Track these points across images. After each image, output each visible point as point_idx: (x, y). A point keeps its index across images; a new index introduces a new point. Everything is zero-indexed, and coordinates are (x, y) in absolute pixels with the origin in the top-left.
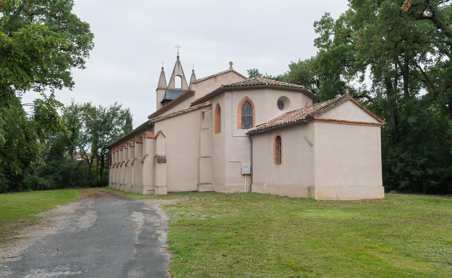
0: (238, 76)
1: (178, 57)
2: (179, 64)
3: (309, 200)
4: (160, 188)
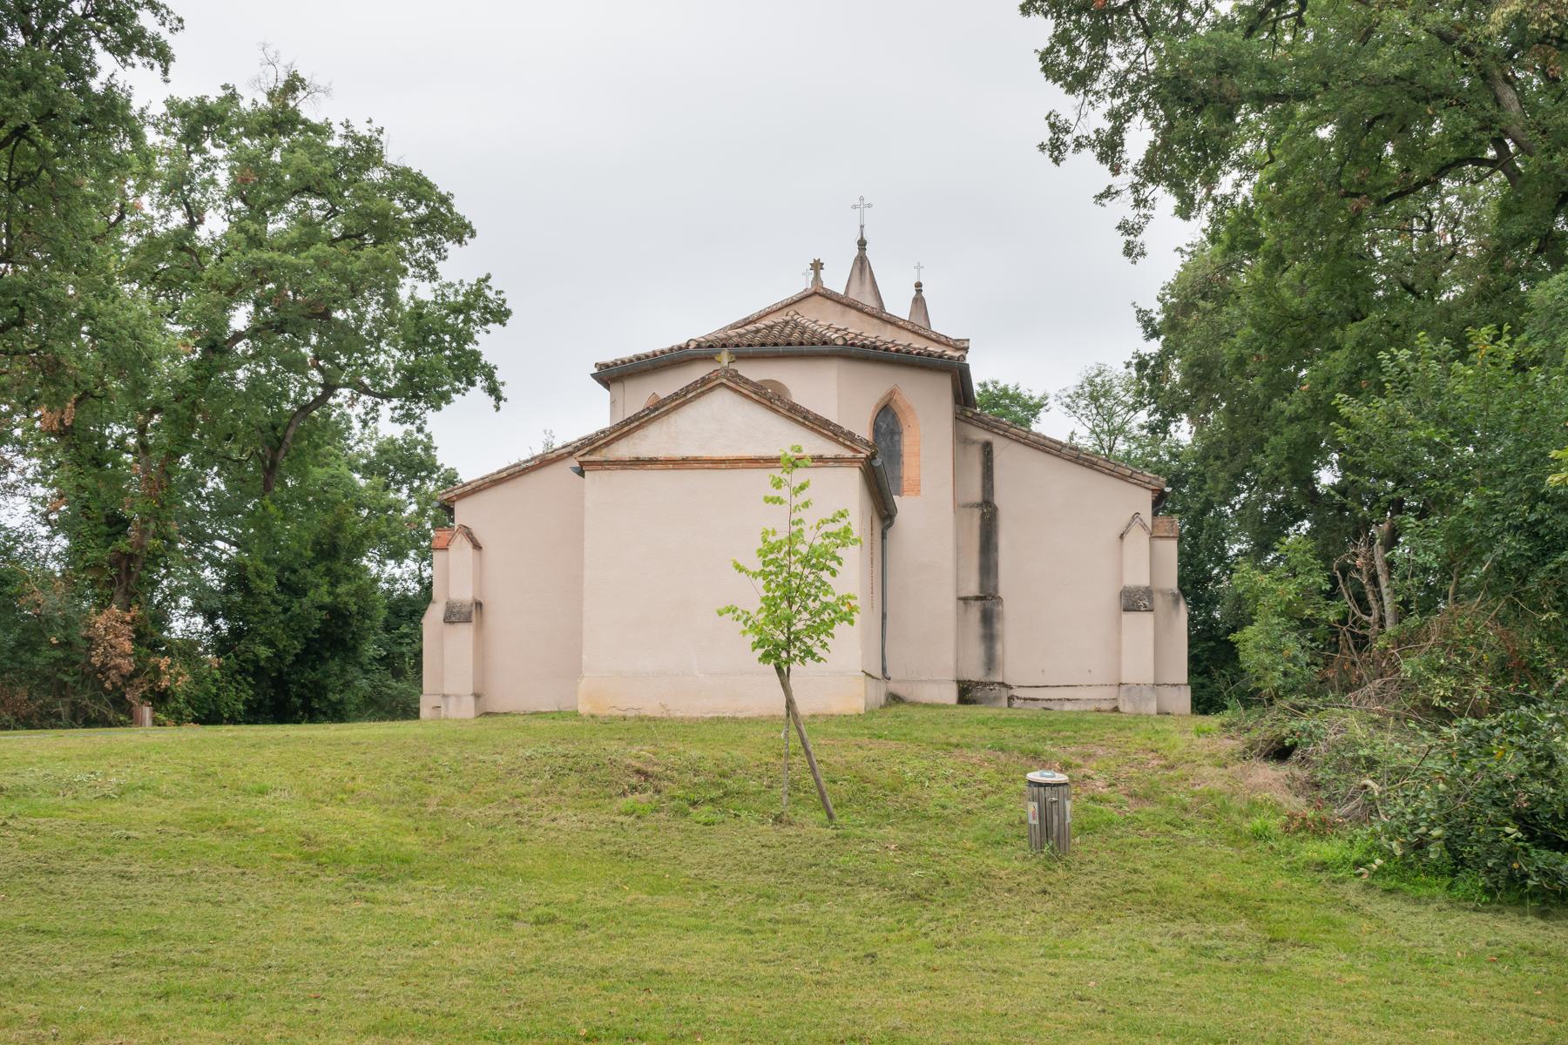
0: (839, 307)
1: (862, 244)
2: (862, 270)
3: (576, 715)
4: (452, 701)
